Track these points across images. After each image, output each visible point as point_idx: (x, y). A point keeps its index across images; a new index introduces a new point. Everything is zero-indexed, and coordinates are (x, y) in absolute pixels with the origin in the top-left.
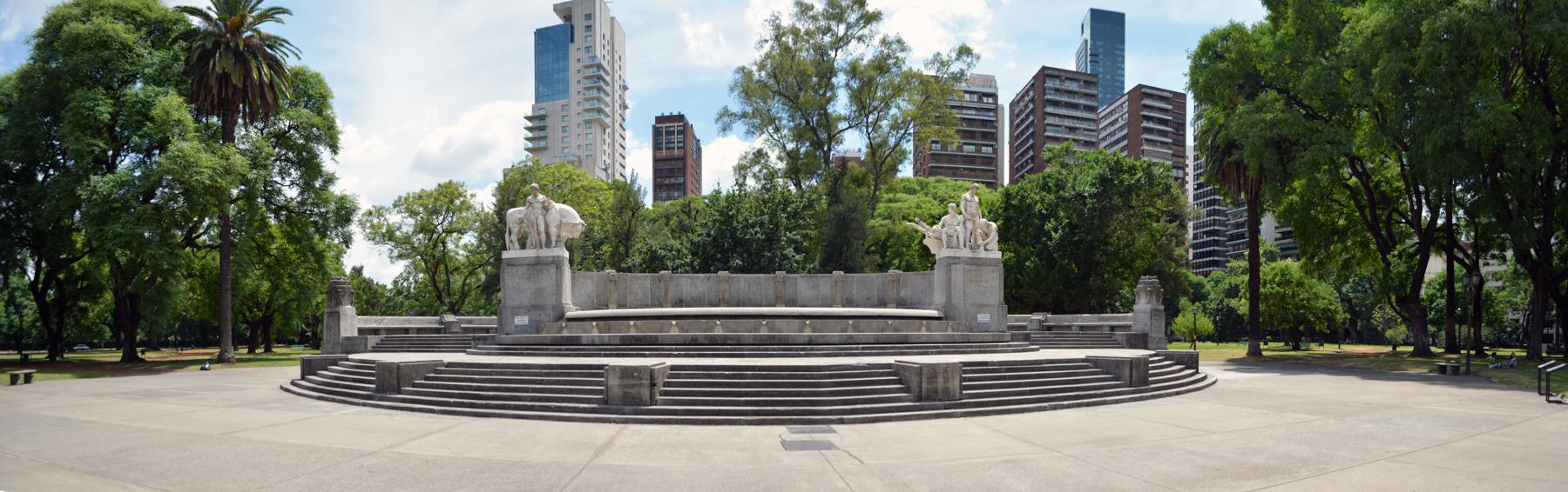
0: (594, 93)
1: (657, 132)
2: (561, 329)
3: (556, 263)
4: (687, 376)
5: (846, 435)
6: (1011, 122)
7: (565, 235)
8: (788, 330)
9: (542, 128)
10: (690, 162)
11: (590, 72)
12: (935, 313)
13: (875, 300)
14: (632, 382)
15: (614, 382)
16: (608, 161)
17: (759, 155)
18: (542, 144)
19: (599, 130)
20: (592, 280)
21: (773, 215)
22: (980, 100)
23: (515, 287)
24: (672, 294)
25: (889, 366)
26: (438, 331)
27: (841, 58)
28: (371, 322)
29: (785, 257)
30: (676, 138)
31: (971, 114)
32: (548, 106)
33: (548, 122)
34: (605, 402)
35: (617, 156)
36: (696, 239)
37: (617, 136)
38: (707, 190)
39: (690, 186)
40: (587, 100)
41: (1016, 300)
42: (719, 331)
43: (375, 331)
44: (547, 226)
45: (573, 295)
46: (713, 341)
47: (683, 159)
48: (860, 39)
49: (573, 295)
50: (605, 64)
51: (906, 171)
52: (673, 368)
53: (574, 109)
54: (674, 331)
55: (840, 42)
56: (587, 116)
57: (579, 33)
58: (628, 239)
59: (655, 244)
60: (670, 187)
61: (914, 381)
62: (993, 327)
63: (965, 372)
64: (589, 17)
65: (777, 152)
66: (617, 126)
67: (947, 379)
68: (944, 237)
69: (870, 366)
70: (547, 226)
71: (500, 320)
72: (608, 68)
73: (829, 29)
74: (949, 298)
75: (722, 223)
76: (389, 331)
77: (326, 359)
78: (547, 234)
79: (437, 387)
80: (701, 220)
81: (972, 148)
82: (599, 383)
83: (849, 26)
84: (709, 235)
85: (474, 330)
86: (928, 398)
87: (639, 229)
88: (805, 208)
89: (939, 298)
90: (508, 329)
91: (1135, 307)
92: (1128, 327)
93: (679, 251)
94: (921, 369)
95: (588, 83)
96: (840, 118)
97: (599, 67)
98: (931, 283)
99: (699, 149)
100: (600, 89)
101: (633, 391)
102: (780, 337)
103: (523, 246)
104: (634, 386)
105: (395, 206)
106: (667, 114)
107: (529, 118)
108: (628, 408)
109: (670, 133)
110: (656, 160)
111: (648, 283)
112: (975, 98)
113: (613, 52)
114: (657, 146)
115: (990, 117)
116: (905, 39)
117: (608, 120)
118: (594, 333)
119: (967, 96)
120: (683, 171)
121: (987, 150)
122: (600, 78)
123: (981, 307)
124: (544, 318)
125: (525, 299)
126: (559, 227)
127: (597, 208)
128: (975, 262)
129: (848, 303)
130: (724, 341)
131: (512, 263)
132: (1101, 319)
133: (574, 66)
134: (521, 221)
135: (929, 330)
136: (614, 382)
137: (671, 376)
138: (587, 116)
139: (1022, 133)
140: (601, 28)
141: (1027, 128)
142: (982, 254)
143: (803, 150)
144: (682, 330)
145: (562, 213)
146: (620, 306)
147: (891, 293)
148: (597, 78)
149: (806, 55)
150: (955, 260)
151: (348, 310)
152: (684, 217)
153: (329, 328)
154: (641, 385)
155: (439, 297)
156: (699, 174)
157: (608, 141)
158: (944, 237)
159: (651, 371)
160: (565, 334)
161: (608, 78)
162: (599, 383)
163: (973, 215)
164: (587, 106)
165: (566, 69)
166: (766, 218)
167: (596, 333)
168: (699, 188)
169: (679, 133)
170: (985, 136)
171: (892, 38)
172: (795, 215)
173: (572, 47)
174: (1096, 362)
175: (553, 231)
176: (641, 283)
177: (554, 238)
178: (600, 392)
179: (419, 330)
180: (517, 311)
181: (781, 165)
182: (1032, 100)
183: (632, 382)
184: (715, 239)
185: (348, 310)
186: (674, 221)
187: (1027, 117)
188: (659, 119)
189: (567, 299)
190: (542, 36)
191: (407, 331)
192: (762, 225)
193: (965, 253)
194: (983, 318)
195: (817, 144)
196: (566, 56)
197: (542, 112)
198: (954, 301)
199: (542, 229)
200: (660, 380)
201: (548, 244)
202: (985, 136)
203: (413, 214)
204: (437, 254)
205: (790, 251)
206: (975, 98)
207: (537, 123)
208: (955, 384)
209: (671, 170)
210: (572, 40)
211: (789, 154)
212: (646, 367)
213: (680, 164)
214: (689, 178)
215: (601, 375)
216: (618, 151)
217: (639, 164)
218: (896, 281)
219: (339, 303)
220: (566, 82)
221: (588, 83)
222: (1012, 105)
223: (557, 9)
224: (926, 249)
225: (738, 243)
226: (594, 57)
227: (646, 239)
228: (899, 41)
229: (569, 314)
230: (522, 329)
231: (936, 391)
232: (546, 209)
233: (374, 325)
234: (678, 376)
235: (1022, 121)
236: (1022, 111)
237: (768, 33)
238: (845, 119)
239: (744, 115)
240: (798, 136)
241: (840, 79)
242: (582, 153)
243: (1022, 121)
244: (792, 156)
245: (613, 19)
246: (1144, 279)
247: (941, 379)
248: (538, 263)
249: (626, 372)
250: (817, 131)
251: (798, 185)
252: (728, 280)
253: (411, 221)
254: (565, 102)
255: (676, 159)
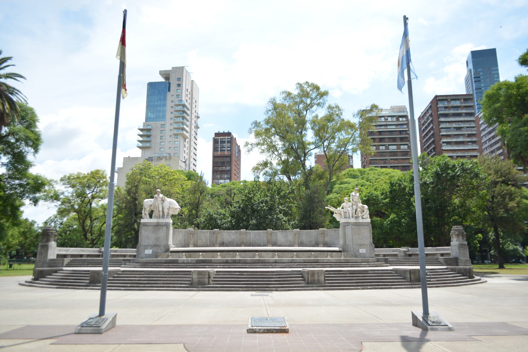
0: (180, 120)
1: (215, 141)
2: (168, 256)
3: (167, 225)
4: (222, 275)
5: (270, 294)
6: (420, 129)
7: (171, 213)
8: (268, 257)
9: (149, 136)
10: (234, 158)
11: (179, 108)
12: (337, 249)
13: (313, 243)
14: (201, 276)
15: (195, 276)
16: (187, 157)
17: (265, 164)
18: (148, 145)
19: (182, 140)
20: (182, 233)
21: (272, 197)
22: (398, 120)
23: (146, 236)
24: (219, 240)
25: (300, 271)
26: (98, 256)
27: (309, 116)
28: (64, 251)
29: (278, 219)
30: (226, 145)
31: (393, 128)
32: (152, 124)
33: (152, 133)
34: (192, 284)
35: (192, 154)
36: (233, 209)
37: (192, 143)
38: (242, 178)
39: (233, 172)
40: (176, 123)
41: (378, 242)
42: (238, 258)
43: (65, 256)
44: (163, 209)
45: (174, 240)
46: (235, 262)
47: (230, 156)
48: (318, 104)
49: (174, 240)
50: (187, 104)
51: (357, 163)
52: (217, 272)
53: (168, 127)
54: (219, 257)
55: (308, 107)
56: (176, 132)
57: (173, 87)
58: (198, 207)
59: (211, 211)
60: (222, 172)
61: (306, 276)
62: (368, 255)
63: (326, 274)
64: (179, 79)
65: (277, 161)
66: (193, 138)
67: (318, 276)
68: (342, 213)
69: (292, 271)
70: (163, 209)
71: (137, 252)
72: (189, 107)
73: (302, 102)
74: (345, 242)
75: (246, 201)
76: (72, 256)
77: (51, 270)
78: (163, 212)
79: (120, 280)
80: (236, 199)
81: (395, 147)
82: (188, 277)
83: (312, 99)
84: (239, 207)
85: (118, 256)
86: (311, 283)
87: (204, 202)
88: (289, 193)
89: (341, 242)
90: (141, 256)
91: (452, 243)
92: (449, 254)
93: (224, 215)
94: (308, 272)
95: (177, 114)
96: (309, 144)
97: (184, 106)
98: (338, 234)
99: (239, 151)
100: (183, 118)
101: (202, 280)
102: (262, 260)
103: (151, 216)
104: (202, 278)
105: (62, 180)
106: (221, 132)
107: (141, 130)
108: (200, 286)
109: (223, 142)
110: (214, 157)
111: (208, 235)
112: (395, 119)
113: (192, 98)
114: (215, 149)
115: (404, 128)
116: (340, 106)
117: (187, 135)
118: (183, 258)
119: (390, 119)
120: (230, 163)
121: (404, 148)
122: (184, 112)
123: (361, 246)
124: (159, 251)
125: (151, 242)
126: (169, 209)
127: (181, 190)
128: (357, 224)
129: (301, 244)
130: (239, 262)
131: (145, 225)
132: (437, 250)
133: (169, 104)
134: (151, 205)
135: (331, 257)
136: (195, 276)
137: (216, 275)
138: (176, 132)
139: (427, 134)
140: (186, 85)
141: (429, 131)
142: (361, 220)
143: (291, 160)
144: (222, 257)
145: (170, 203)
146: (195, 245)
147: (321, 239)
148: (182, 112)
149: (291, 115)
150: (347, 224)
151: (53, 244)
152: (228, 197)
153: (41, 254)
154: (205, 278)
155: (85, 235)
156: (239, 169)
157: (187, 145)
158: (342, 213)
159: (209, 273)
160: (170, 258)
161: (188, 112)
162: (188, 277)
163: (356, 202)
164: (176, 126)
165: (164, 105)
166: (268, 199)
167: (184, 258)
168: (239, 177)
169: (228, 142)
170: (402, 139)
171: (333, 105)
172: (284, 197)
173: (169, 94)
174: (396, 271)
175: (166, 211)
176: (205, 234)
177: (166, 214)
178: (190, 281)
179: (88, 256)
180: (146, 247)
181: (279, 168)
182: (431, 115)
183: (201, 276)
184: (243, 209)
185: (53, 244)
186: (222, 198)
187: (429, 125)
188: (217, 135)
189: (170, 242)
190: (152, 86)
191: (81, 256)
192: (266, 202)
193: (352, 220)
194: (362, 251)
195: (298, 157)
196: (165, 99)
197: (149, 127)
198: (347, 243)
199: (161, 209)
200: (212, 276)
201: (163, 217)
202: (402, 139)
203: (73, 186)
204: (87, 210)
205: (281, 216)
206: (395, 119)
207: (145, 133)
208: (322, 278)
209: (223, 163)
210: (169, 90)
211: (283, 162)
212: (207, 271)
213: (228, 159)
214: (233, 167)
215: (190, 275)
216: (193, 150)
217: (204, 167)
218: (323, 233)
219: (48, 240)
220: (164, 112)
221: (177, 114)
222: (419, 119)
223: (162, 73)
224: (334, 219)
225: (254, 211)
226: (181, 100)
227: (210, 208)
228: (337, 107)
229: (172, 249)
230: (149, 256)
231: (314, 281)
232: (163, 201)
233: (64, 253)
234: (219, 275)
235: (426, 128)
236: (425, 122)
237: (271, 107)
238: (313, 143)
239: (258, 144)
240: (287, 151)
241: (308, 125)
242: (172, 152)
243: (426, 128)
244: (285, 163)
245: (192, 81)
246: (454, 227)
247: (316, 276)
248: (158, 225)
249: (199, 273)
250: (297, 151)
251: (289, 178)
252: (245, 234)
253: (71, 190)
254: (163, 123)
255: (226, 157)
